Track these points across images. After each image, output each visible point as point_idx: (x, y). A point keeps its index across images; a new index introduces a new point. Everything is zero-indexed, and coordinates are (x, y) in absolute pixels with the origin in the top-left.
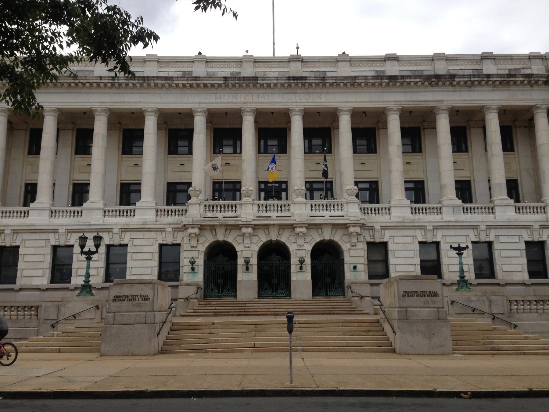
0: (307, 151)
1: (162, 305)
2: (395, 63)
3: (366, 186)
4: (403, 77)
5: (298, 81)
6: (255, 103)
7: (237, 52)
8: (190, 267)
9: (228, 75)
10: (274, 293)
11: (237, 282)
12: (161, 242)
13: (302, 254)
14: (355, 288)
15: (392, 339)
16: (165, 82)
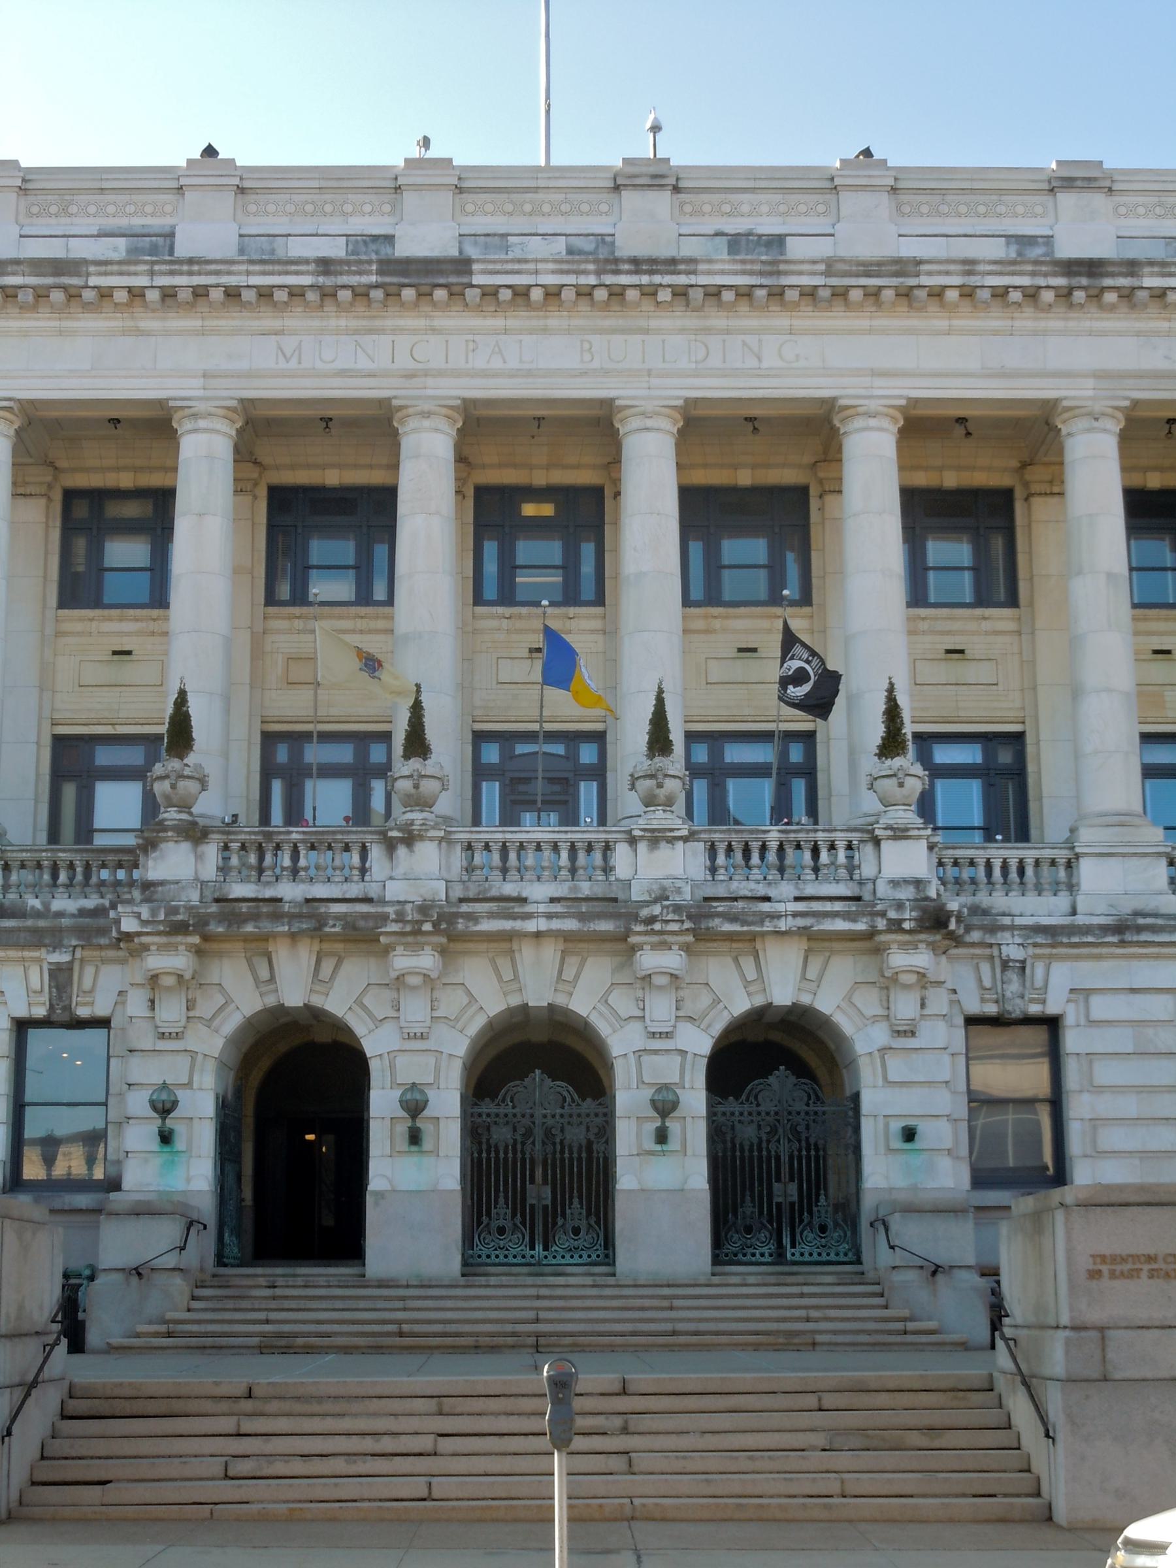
0: (697, 593)
1: (21, 1308)
2: (1098, 200)
3: (969, 755)
4: (1132, 267)
5: (657, 279)
6: (457, 374)
7: (91, 1128)
8: (153, 1127)
9: (336, 249)
10: (539, 1247)
11: (369, 1200)
12: (22, 1012)
13: (666, 1070)
14: (908, 1231)
15: (1039, 1466)
16: (49, 281)
